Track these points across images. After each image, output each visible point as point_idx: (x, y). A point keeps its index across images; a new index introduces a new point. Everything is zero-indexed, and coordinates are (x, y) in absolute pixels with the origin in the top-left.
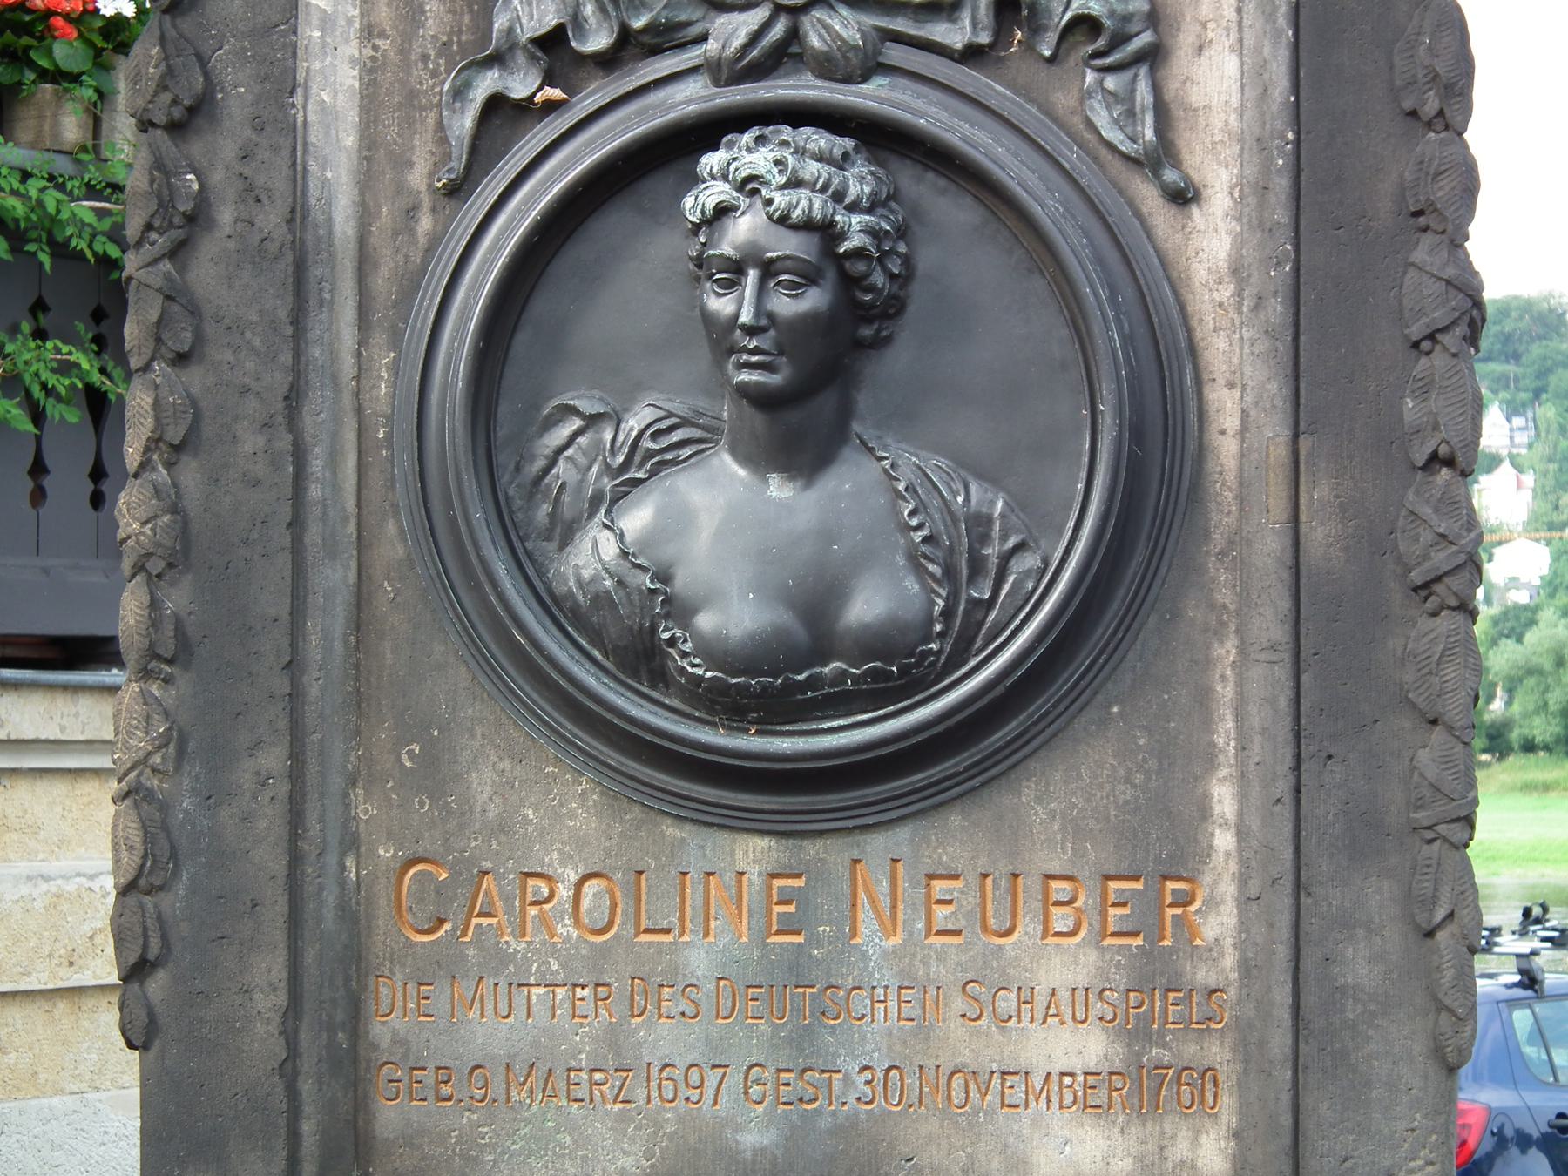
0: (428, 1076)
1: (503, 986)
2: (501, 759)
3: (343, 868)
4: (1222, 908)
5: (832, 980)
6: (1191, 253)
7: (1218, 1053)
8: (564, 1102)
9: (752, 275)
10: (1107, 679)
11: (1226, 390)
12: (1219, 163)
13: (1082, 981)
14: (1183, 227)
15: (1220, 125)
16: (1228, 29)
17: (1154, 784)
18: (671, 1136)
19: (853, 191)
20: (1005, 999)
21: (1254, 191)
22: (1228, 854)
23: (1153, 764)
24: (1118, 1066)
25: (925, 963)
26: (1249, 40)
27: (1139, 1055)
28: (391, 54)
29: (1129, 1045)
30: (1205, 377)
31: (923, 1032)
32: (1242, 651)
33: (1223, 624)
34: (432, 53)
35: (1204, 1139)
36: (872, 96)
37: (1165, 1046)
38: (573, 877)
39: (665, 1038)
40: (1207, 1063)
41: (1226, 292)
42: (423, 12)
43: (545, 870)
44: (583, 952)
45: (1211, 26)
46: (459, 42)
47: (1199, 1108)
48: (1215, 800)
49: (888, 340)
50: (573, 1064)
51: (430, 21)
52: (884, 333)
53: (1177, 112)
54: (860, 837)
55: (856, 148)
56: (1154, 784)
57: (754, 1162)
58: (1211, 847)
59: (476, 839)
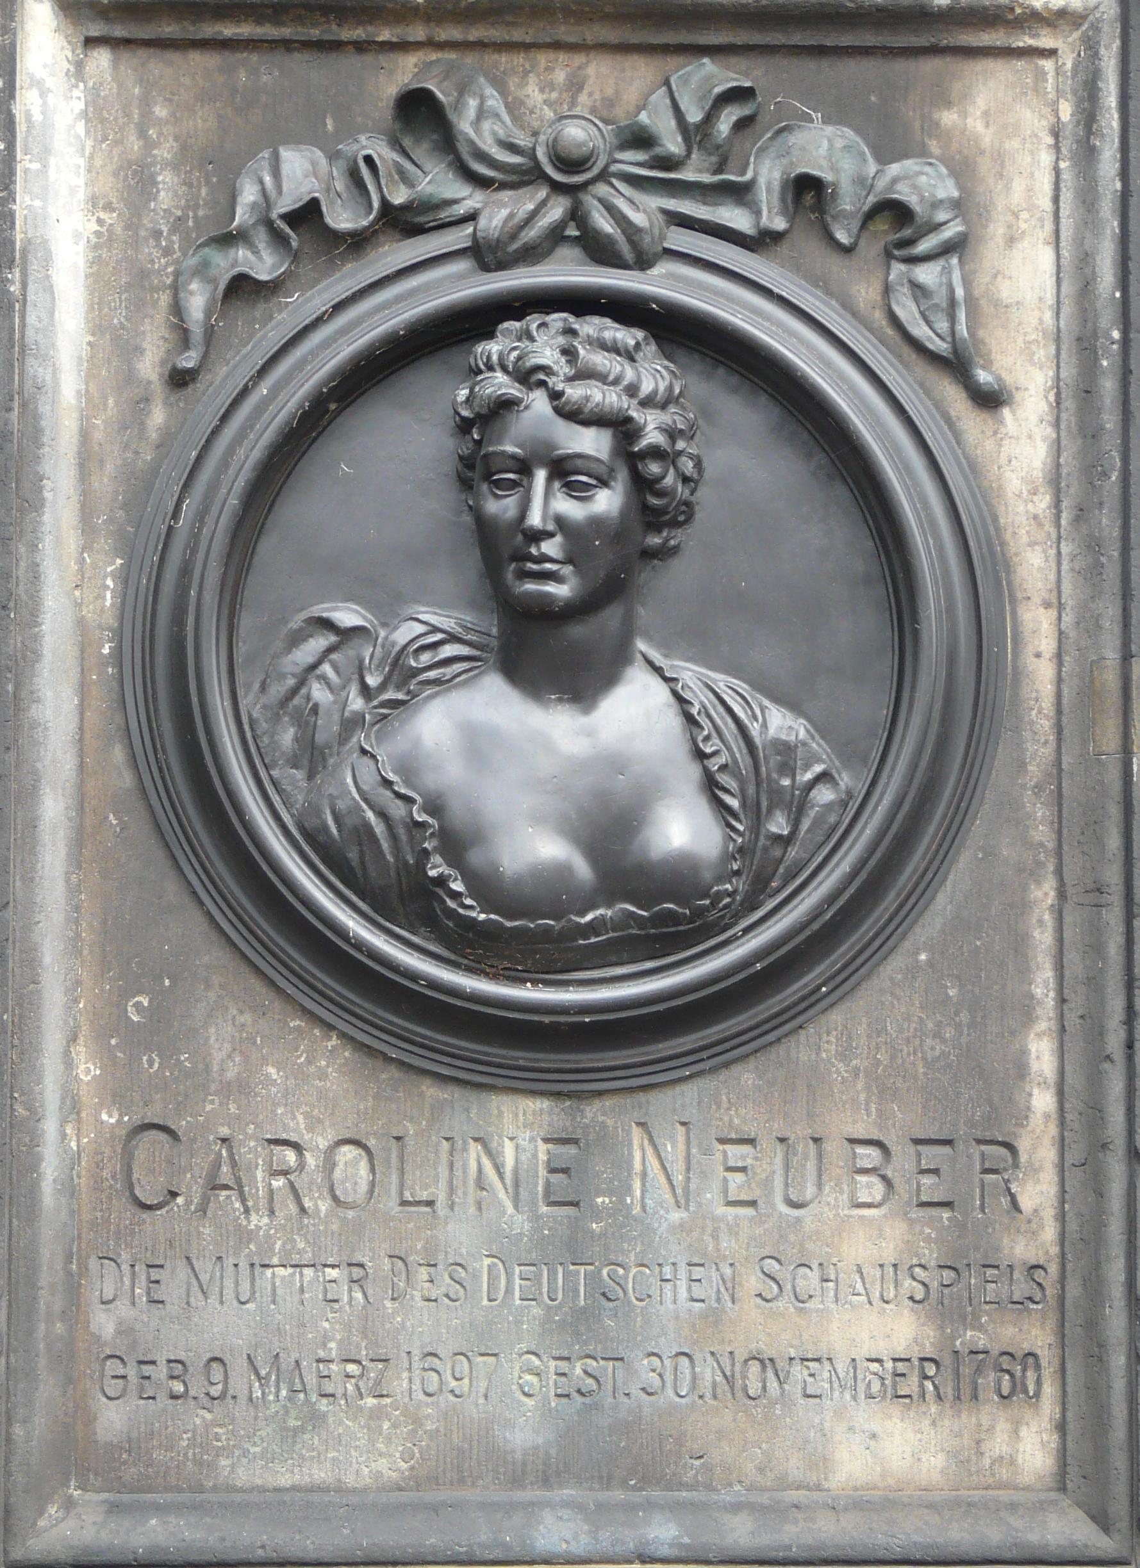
0: (160, 1372)
1: (244, 1265)
2: (241, 1012)
3: (64, 1136)
4: (1042, 1175)
5: (612, 1257)
6: (1003, 460)
7: (1038, 1337)
8: (314, 1397)
9: (541, 475)
10: (915, 922)
11: (1042, 610)
12: (1034, 364)
13: (889, 1256)
14: (995, 433)
15: (1035, 322)
16: (1041, 220)
17: (964, 1039)
18: (433, 1435)
19: (647, 387)
20: (805, 1277)
21: (1077, 398)
22: (1047, 1116)
23: (964, 1017)
24: (929, 1352)
25: (715, 1237)
26: (1066, 233)
27: (953, 1338)
28: (118, 230)
29: (942, 1328)
30: (1019, 595)
31: (714, 1318)
32: (1062, 894)
33: (1040, 864)
34: (165, 229)
35: (1024, 1432)
36: (658, 283)
37: (980, 1328)
38: (323, 1143)
39: (418, 1321)
40: (1026, 1347)
41: (1043, 503)
42: (155, 183)
43: (293, 1137)
44: (335, 1227)
45: (1024, 215)
46: (195, 217)
47: (1015, 1394)
48: (1033, 1056)
49: (675, 550)
50: (322, 1354)
51: (162, 193)
52: (672, 542)
53: (986, 307)
54: (642, 1097)
55: (645, 338)
56: (964, 1039)
57: (524, 1464)
58: (1029, 1108)
59: (212, 1102)
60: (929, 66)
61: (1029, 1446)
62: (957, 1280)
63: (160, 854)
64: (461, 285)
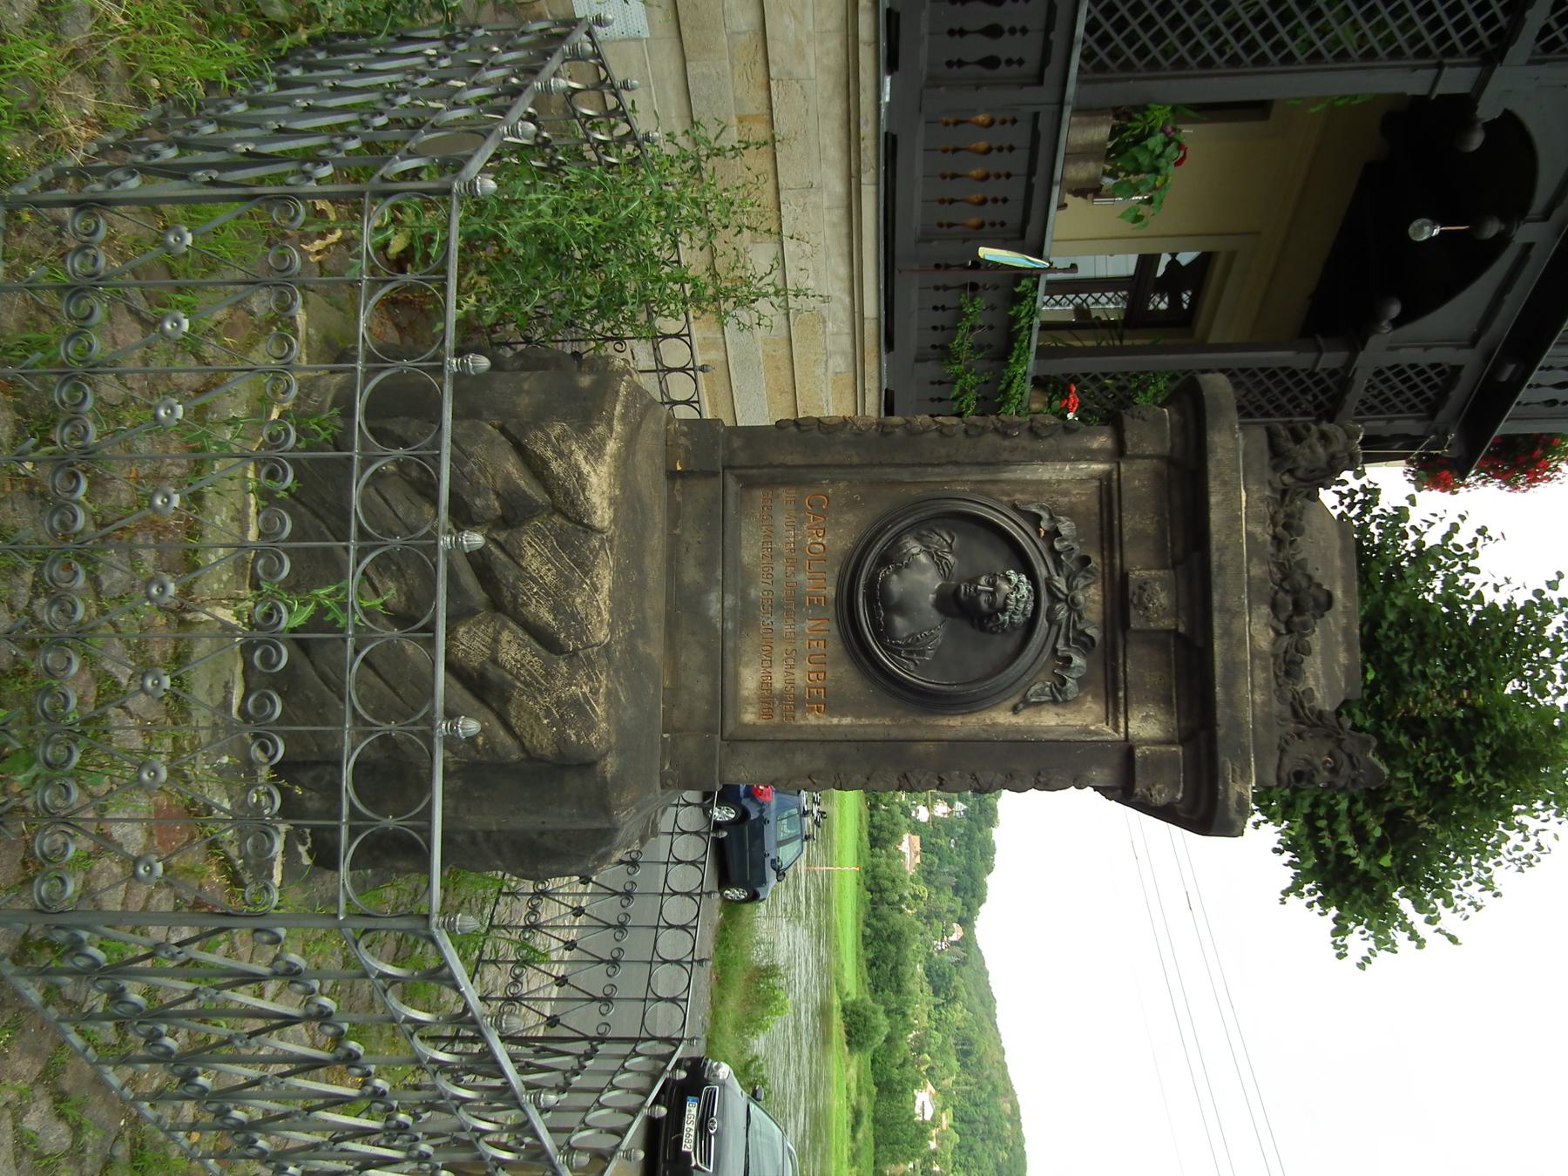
7: (777, 719)
21: (1017, 729)
36: (1043, 622)
60: (1102, 692)
61: (749, 717)
62: (796, 701)
63: (845, 141)
64: (1042, 572)
